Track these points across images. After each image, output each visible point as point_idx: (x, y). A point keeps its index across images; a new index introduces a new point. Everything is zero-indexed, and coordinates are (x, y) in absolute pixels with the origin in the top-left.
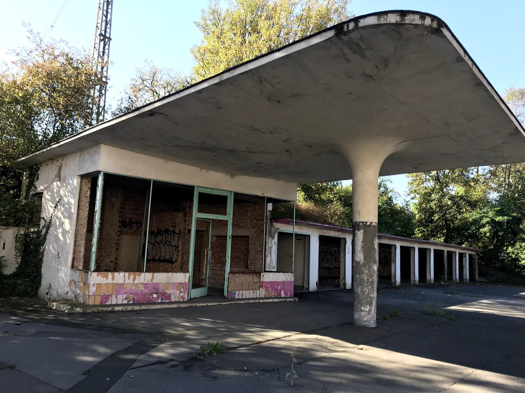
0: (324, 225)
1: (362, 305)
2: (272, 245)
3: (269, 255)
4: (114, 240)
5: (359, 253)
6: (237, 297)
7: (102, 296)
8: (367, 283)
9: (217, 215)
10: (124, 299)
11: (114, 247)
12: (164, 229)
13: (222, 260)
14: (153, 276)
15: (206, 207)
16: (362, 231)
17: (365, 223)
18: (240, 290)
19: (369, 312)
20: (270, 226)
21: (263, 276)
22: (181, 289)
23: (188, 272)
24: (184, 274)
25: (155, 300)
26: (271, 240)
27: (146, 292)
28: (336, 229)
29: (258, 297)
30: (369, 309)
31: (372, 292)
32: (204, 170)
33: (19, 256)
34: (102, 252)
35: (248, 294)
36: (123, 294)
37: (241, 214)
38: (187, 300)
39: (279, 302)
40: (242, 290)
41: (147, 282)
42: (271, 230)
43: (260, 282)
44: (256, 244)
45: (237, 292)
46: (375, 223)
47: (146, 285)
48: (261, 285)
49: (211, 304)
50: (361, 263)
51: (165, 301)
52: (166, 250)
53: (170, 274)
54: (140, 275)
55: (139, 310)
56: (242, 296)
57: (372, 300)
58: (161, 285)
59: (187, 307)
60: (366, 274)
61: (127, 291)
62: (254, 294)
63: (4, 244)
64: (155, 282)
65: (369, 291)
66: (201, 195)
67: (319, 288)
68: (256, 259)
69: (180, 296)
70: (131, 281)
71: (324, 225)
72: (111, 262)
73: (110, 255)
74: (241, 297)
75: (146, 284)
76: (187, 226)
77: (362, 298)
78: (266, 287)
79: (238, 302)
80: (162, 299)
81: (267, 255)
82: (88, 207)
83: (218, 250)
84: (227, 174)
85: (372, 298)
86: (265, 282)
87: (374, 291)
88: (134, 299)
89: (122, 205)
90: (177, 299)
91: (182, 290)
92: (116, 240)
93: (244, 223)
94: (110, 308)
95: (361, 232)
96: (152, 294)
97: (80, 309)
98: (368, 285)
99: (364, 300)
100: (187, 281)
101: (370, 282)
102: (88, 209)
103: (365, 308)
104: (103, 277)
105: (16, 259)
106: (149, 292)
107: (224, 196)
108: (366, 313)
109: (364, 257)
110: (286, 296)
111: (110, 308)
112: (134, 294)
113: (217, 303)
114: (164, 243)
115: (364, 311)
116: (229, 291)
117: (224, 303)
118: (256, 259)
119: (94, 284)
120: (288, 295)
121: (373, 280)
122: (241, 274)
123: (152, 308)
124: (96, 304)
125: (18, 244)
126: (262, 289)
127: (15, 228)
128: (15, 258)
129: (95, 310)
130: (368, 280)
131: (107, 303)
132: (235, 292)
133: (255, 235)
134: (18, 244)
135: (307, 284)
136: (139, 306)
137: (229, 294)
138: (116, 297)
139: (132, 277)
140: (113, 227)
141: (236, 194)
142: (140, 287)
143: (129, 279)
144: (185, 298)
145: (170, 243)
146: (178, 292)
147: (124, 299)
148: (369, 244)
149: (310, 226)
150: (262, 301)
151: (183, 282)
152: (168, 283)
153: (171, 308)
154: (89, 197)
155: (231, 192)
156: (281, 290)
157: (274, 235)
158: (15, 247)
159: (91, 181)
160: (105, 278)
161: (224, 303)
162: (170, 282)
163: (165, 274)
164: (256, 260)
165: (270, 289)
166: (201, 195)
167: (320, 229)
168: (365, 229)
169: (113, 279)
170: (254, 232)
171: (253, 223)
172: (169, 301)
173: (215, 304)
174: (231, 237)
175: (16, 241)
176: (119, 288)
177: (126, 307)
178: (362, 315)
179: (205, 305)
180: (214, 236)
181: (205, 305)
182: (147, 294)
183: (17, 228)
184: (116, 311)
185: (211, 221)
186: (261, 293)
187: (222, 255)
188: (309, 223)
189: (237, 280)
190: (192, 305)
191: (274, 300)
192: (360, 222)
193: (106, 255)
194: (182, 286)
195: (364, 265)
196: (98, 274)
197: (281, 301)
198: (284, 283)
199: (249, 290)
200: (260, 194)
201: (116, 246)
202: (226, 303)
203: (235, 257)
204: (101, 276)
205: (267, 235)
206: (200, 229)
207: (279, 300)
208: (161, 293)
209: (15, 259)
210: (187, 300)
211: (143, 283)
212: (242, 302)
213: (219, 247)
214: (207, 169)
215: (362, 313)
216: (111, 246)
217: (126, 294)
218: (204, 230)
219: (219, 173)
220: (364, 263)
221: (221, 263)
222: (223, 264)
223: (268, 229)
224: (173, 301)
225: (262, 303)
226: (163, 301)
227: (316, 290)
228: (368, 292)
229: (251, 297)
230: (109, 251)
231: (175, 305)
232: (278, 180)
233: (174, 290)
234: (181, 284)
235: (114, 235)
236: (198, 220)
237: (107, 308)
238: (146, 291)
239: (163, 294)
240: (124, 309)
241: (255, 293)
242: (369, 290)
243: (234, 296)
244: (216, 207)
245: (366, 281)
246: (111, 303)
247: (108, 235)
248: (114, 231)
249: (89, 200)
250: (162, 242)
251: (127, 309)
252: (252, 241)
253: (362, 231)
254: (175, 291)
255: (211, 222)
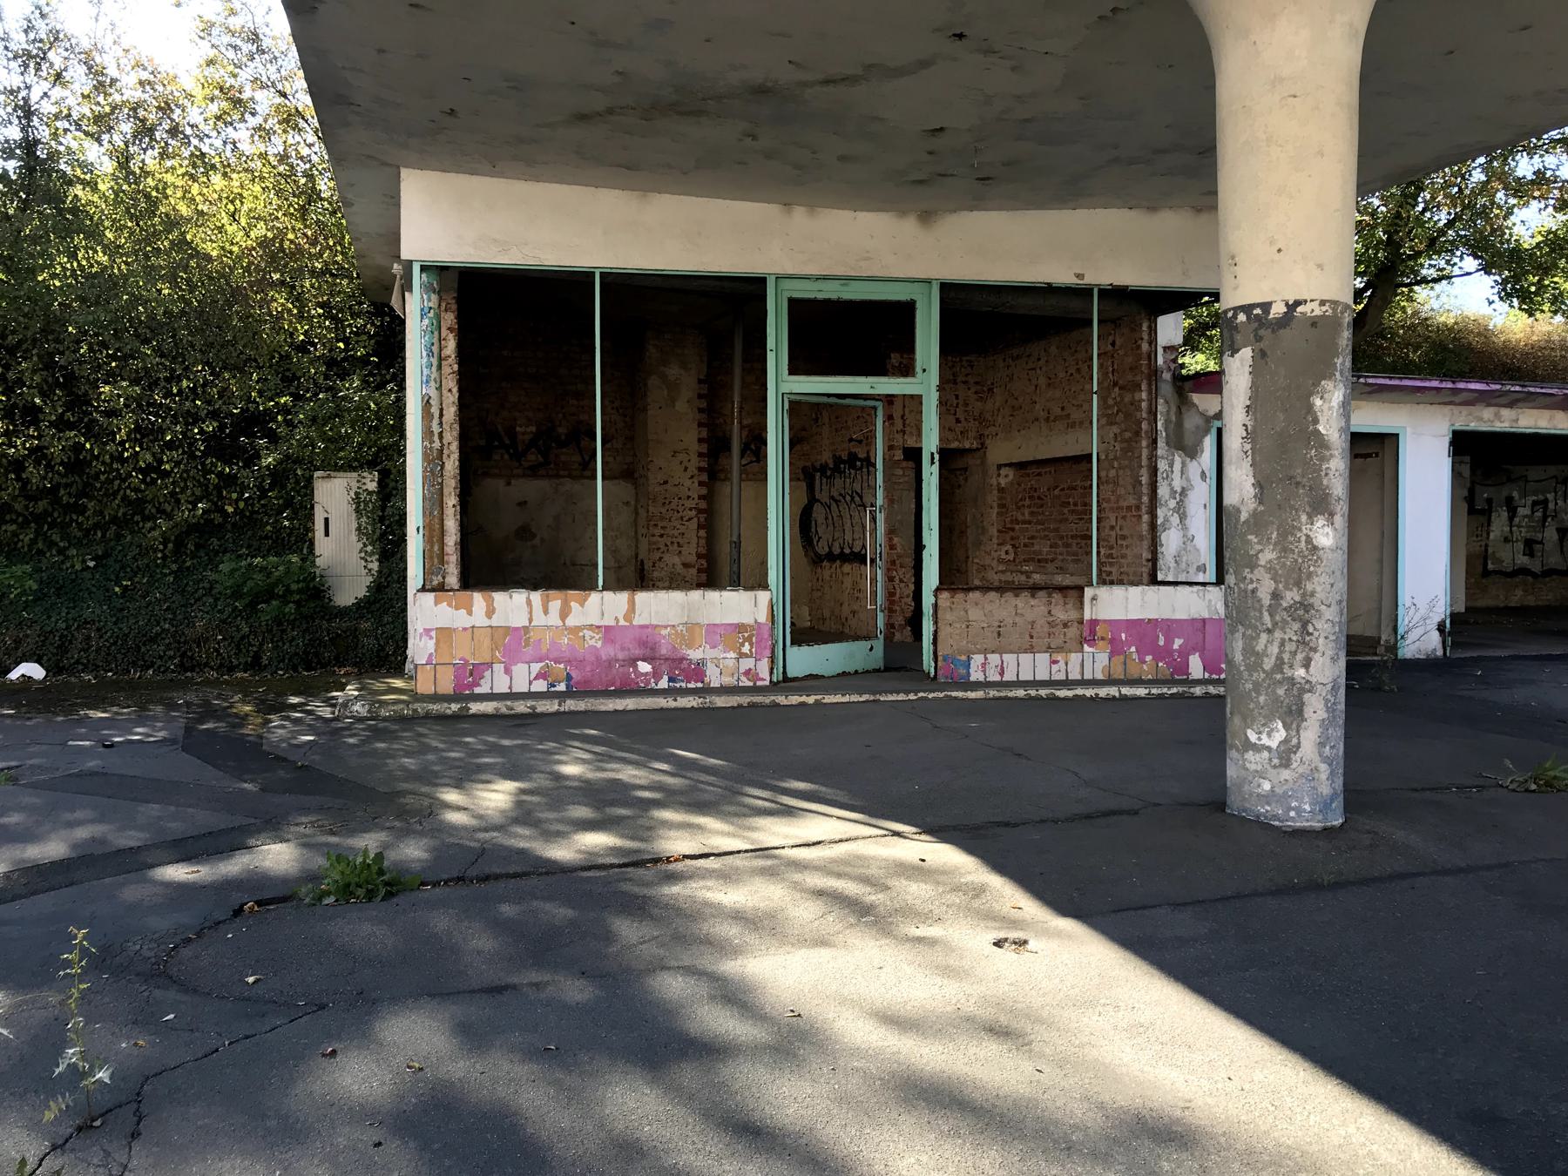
0: (1461, 385)
1: (1248, 720)
2: (1188, 480)
3: (1175, 519)
4: (689, 497)
5: (1233, 467)
6: (976, 675)
7: (459, 668)
8: (1272, 611)
9: (871, 379)
10: (536, 678)
11: (690, 519)
12: (847, 453)
13: (1036, 547)
14: (632, 603)
15: (972, 367)
16: (1246, 353)
17: (1258, 311)
18: (993, 652)
19: (1286, 755)
20: (1174, 409)
21: (1094, 598)
22: (742, 645)
23: (764, 586)
24: (750, 594)
25: (648, 683)
26: (1184, 464)
27: (612, 654)
28: (1548, 399)
29: (1075, 675)
30: (1286, 741)
31: (1300, 657)
32: (799, 213)
33: (372, 554)
34: (653, 536)
35: (1033, 666)
36: (528, 663)
37: (1072, 374)
38: (767, 683)
39: (1150, 698)
40: (1000, 651)
41: (612, 623)
42: (1179, 424)
43: (1081, 622)
44: (1121, 482)
45: (977, 659)
46: (1323, 303)
47: (608, 632)
48: (1089, 633)
49: (838, 699)
50: (1244, 516)
51: (684, 685)
52: (854, 522)
53: (696, 595)
54: (585, 600)
55: (558, 713)
56: (1002, 673)
57: (1300, 696)
58: (664, 632)
59: (740, 706)
60: (1270, 569)
61: (544, 651)
62: (1054, 667)
63: (327, 520)
64: (642, 623)
65: (1281, 652)
66: (800, 310)
67: (1455, 645)
68: (1124, 537)
69: (742, 670)
70: (554, 619)
71: (1461, 385)
72: (686, 565)
73: (679, 545)
74: (997, 678)
75: (608, 629)
76: (899, 437)
77: (1249, 686)
78: (1112, 641)
79: (954, 694)
80: (671, 680)
81: (1166, 520)
82: (455, 390)
83: (1023, 514)
84: (902, 213)
85: (1300, 691)
86: (1105, 621)
87: (1315, 650)
88: (569, 678)
89: (702, 385)
90: (728, 680)
91: (746, 649)
92: (696, 496)
93: (1082, 406)
94: (455, 707)
95: (1242, 360)
96: (633, 662)
97: (363, 705)
98: (1275, 624)
99: (1259, 694)
100: (763, 617)
101: (1285, 609)
102: (457, 396)
103: (1264, 736)
104: (457, 608)
105: (366, 561)
106: (621, 656)
107: (898, 303)
108: (1270, 759)
109: (1259, 485)
110: (1215, 676)
111: (455, 707)
112: (568, 662)
113: (861, 694)
114: (848, 498)
115: (1257, 748)
116: (940, 654)
117: (891, 698)
118: (1124, 537)
119: (427, 631)
120: (1220, 671)
121: (1304, 595)
122: (992, 595)
123: (603, 708)
124: (441, 691)
125: (364, 519)
126: (1091, 650)
127: (349, 474)
128: (361, 558)
129: (403, 709)
130: (1276, 596)
131: (477, 690)
132: (969, 659)
133: (1117, 448)
134: (364, 519)
135: (1390, 629)
136: (556, 701)
137: (940, 664)
138: (508, 671)
139: (555, 605)
140: (681, 457)
141: (947, 288)
142: (587, 638)
143: (546, 612)
144: (761, 676)
145: (861, 497)
146: (732, 655)
147: (536, 678)
148: (1282, 416)
149: (1385, 395)
150: (1070, 694)
151: (748, 620)
152: (691, 627)
153: (676, 709)
154: (453, 356)
155: (928, 282)
156: (1185, 653)
157: (1200, 442)
158: (359, 529)
159: (454, 307)
160: (463, 611)
161: (891, 698)
162: (700, 621)
163: (677, 596)
164: (1125, 543)
165: (1133, 649)
166: (800, 310)
167: (1451, 403)
168: (1259, 339)
169: (490, 612)
170: (1112, 435)
171: (1111, 402)
172: (700, 685)
173: (855, 698)
174: (937, 457)
175: (357, 511)
176: (513, 642)
177: (509, 703)
178: (1248, 765)
179: (811, 700)
180: (1006, 465)
181: (811, 700)
182: (617, 660)
183: (355, 475)
184: (474, 716)
185: (879, 405)
186: (1094, 661)
187: (1038, 531)
188: (1370, 381)
189: (975, 614)
190: (804, 699)
191: (1126, 691)
192: (1237, 310)
193: (666, 545)
194: (746, 635)
195: (1257, 523)
196: (435, 597)
197: (1161, 697)
198: (1200, 625)
199: (1031, 650)
200: (1062, 275)
201: (696, 516)
202: (902, 697)
203: (1072, 537)
204: (450, 605)
205: (1161, 444)
206: (955, 445)
207: (1154, 691)
208: (667, 659)
209: (363, 563)
210: (767, 683)
211: (598, 627)
212: (972, 695)
213: (1027, 502)
214: (812, 206)
215: (1250, 755)
216: (682, 518)
217: (541, 661)
218: (967, 446)
219: (865, 213)
220: (1255, 514)
221: (1032, 560)
222: (1039, 561)
223: (1167, 422)
224: (715, 684)
225: (1065, 699)
226: (678, 685)
227: (1440, 653)
228: (1279, 658)
229: (1046, 677)
230: (676, 533)
231: (691, 698)
232: (1153, 209)
233: (713, 647)
234: (740, 628)
235: (688, 483)
236: (798, 409)
237: (446, 705)
238: (609, 652)
239: (674, 660)
240: (504, 710)
241: (1062, 664)
242: (1282, 644)
243: (963, 671)
244: (1004, 360)
245: (1266, 601)
246: (492, 688)
247: (666, 482)
248: (686, 469)
249: (456, 367)
250: (844, 498)
251: (512, 709)
252: (1108, 471)
253: (1246, 353)
254: (717, 653)
255: (880, 413)
